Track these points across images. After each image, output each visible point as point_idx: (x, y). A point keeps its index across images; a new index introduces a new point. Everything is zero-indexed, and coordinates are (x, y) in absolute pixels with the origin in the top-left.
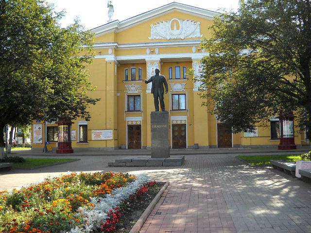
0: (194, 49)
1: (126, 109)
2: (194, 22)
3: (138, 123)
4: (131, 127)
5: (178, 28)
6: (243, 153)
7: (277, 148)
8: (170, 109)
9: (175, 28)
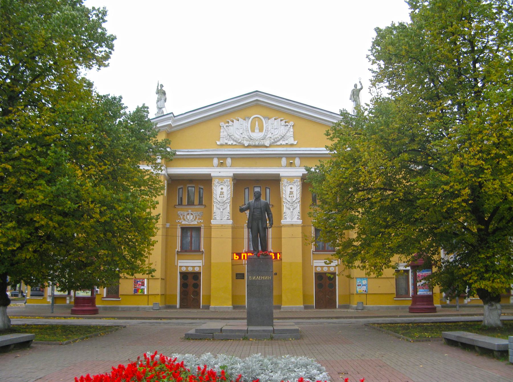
0: (216, 161)
1: (178, 249)
2: (285, 122)
3: (197, 270)
4: (184, 276)
5: (261, 130)
6: (355, 318)
7: (408, 310)
8: (313, 250)
9: (257, 131)
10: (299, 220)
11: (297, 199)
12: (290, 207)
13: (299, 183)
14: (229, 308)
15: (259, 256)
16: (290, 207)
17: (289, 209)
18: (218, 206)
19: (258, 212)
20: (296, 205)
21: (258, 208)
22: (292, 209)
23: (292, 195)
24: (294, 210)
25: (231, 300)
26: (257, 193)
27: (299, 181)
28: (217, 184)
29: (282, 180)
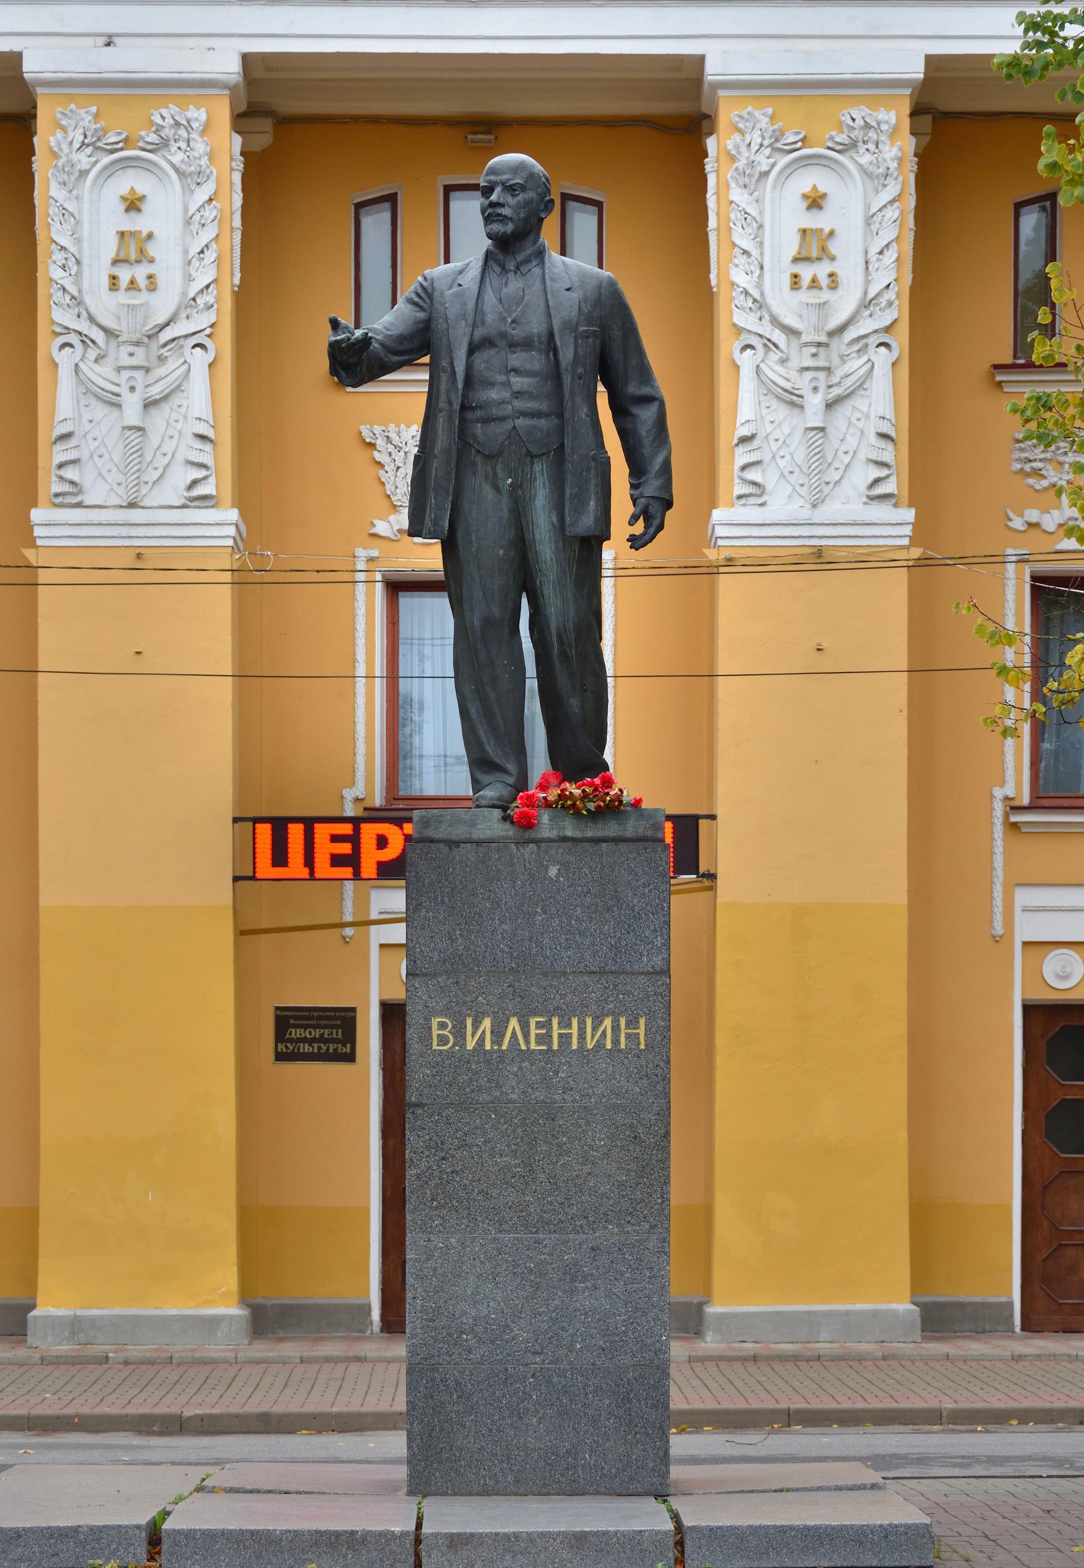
8: (1009, 790)
10: (883, 512)
11: (867, 304)
12: (803, 383)
13: (890, 152)
14: (212, 1323)
15: (526, 823)
16: (803, 383)
17: (793, 401)
18: (100, 374)
19: (518, 382)
20: (856, 364)
21: (526, 344)
22: (815, 402)
23: (822, 270)
24: (844, 411)
25: (231, 1252)
26: (511, 189)
27: (894, 133)
28: (83, 160)
29: (727, 114)
